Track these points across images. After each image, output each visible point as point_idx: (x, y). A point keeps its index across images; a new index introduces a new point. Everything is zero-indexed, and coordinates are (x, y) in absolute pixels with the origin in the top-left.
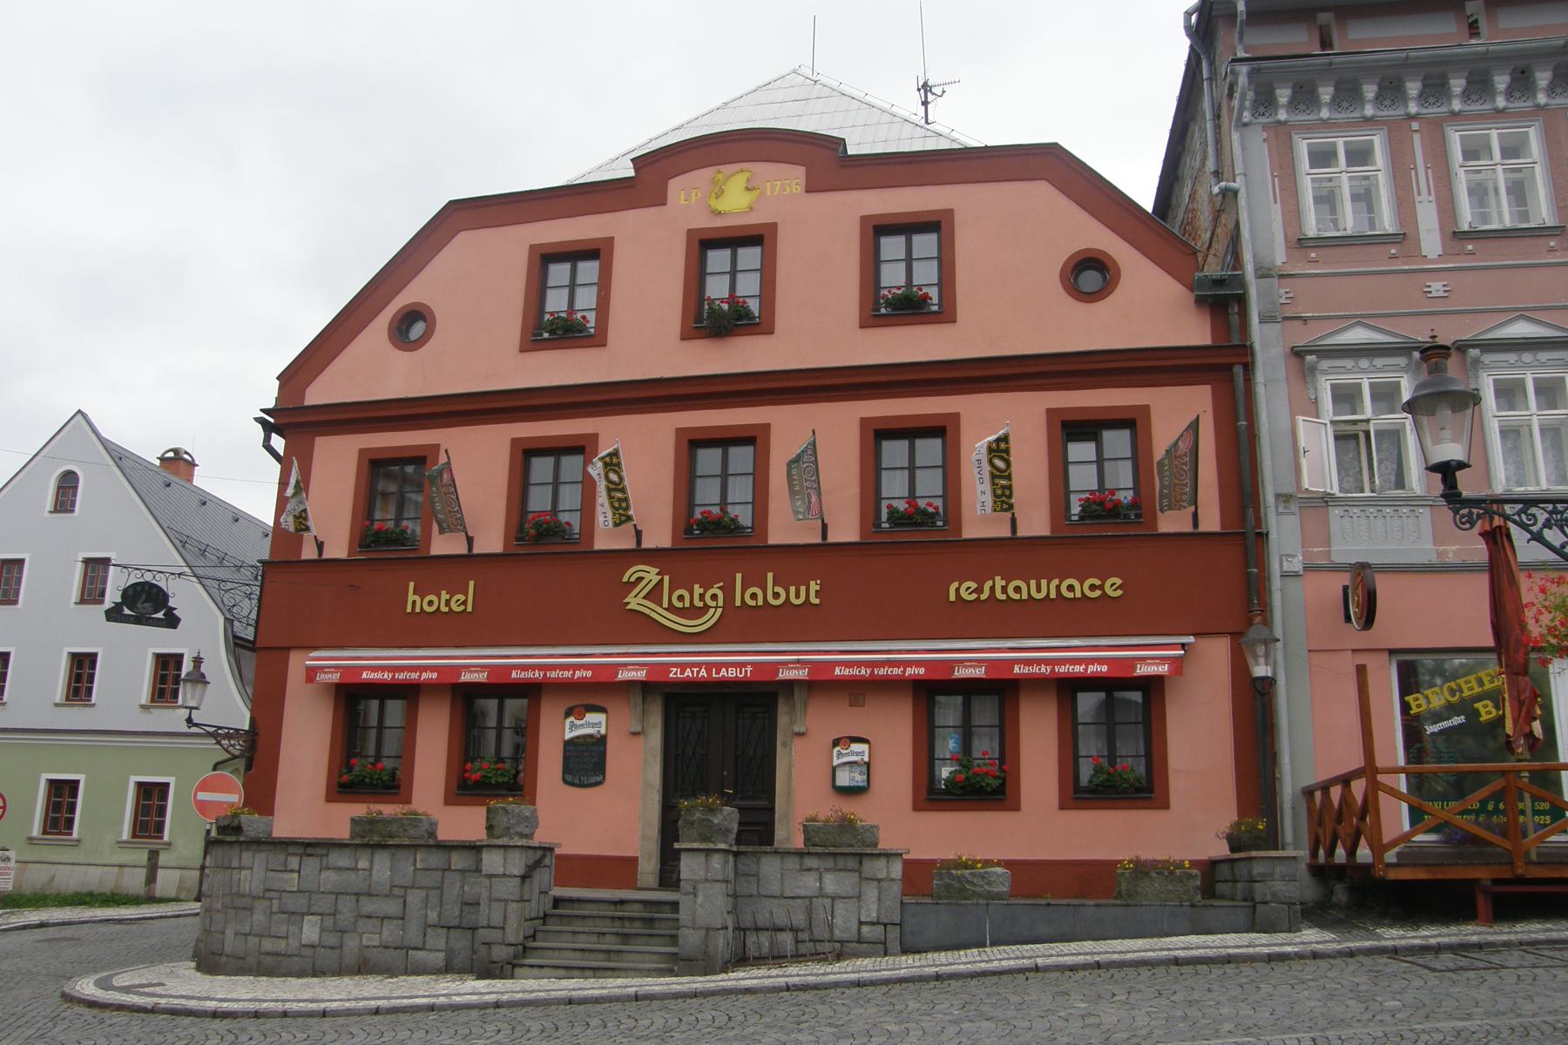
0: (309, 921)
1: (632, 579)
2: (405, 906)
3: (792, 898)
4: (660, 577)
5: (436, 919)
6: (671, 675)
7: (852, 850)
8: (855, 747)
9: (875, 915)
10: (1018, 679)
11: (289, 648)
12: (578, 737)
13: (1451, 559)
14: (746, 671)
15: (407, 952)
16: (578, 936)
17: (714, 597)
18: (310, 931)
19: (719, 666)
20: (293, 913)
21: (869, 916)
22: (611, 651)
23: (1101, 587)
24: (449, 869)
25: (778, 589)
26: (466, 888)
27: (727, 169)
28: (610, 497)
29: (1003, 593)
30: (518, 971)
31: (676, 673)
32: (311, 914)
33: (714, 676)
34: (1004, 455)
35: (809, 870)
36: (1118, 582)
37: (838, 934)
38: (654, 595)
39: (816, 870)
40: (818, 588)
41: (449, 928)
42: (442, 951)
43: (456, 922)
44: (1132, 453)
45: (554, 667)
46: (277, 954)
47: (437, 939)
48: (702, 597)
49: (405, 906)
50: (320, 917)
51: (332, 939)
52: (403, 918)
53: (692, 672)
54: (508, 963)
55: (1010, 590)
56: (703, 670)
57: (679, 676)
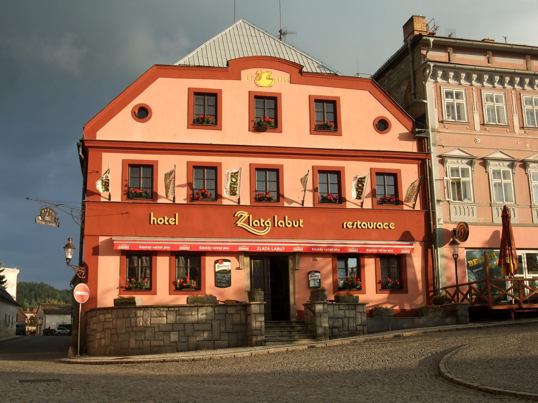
0: (173, 334)
1: (239, 216)
2: (212, 326)
3: (337, 318)
4: (249, 215)
5: (224, 330)
6: (258, 249)
7: (353, 303)
8: (317, 274)
9: (360, 322)
10: (405, 254)
11: (99, 236)
12: (221, 271)
13: (481, 222)
14: (283, 249)
15: (214, 342)
16: (275, 332)
17: (268, 223)
18: (174, 337)
19: (274, 247)
20: (165, 331)
21: (358, 323)
22: (210, 241)
23: (389, 226)
24: (227, 313)
25: (289, 222)
26: (234, 319)
27: (263, 70)
28: (231, 186)
29: (263, 224)
30: (267, 343)
31: (259, 249)
32: (174, 331)
33: (272, 250)
34: (236, 177)
35: (341, 310)
36: (393, 224)
37: (350, 329)
38: (248, 221)
39: (343, 309)
40: (302, 222)
41: (229, 333)
42: (227, 340)
43: (231, 331)
44: (277, 180)
45: (155, 245)
46: (159, 346)
47: (225, 337)
48: (264, 223)
49: (212, 326)
50: (178, 332)
51: (184, 339)
52: (211, 330)
53: (265, 249)
54: (263, 341)
55: (266, 223)
56: (268, 248)
57: (260, 250)
